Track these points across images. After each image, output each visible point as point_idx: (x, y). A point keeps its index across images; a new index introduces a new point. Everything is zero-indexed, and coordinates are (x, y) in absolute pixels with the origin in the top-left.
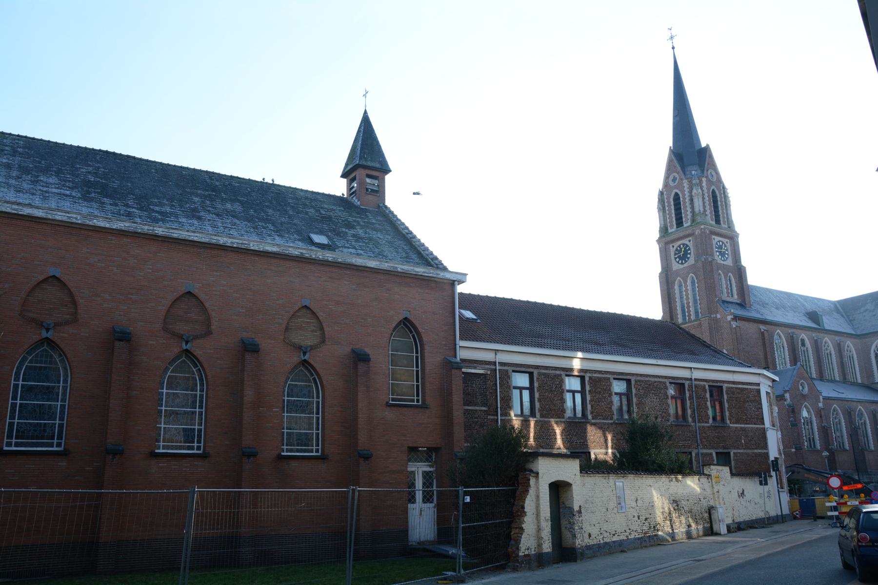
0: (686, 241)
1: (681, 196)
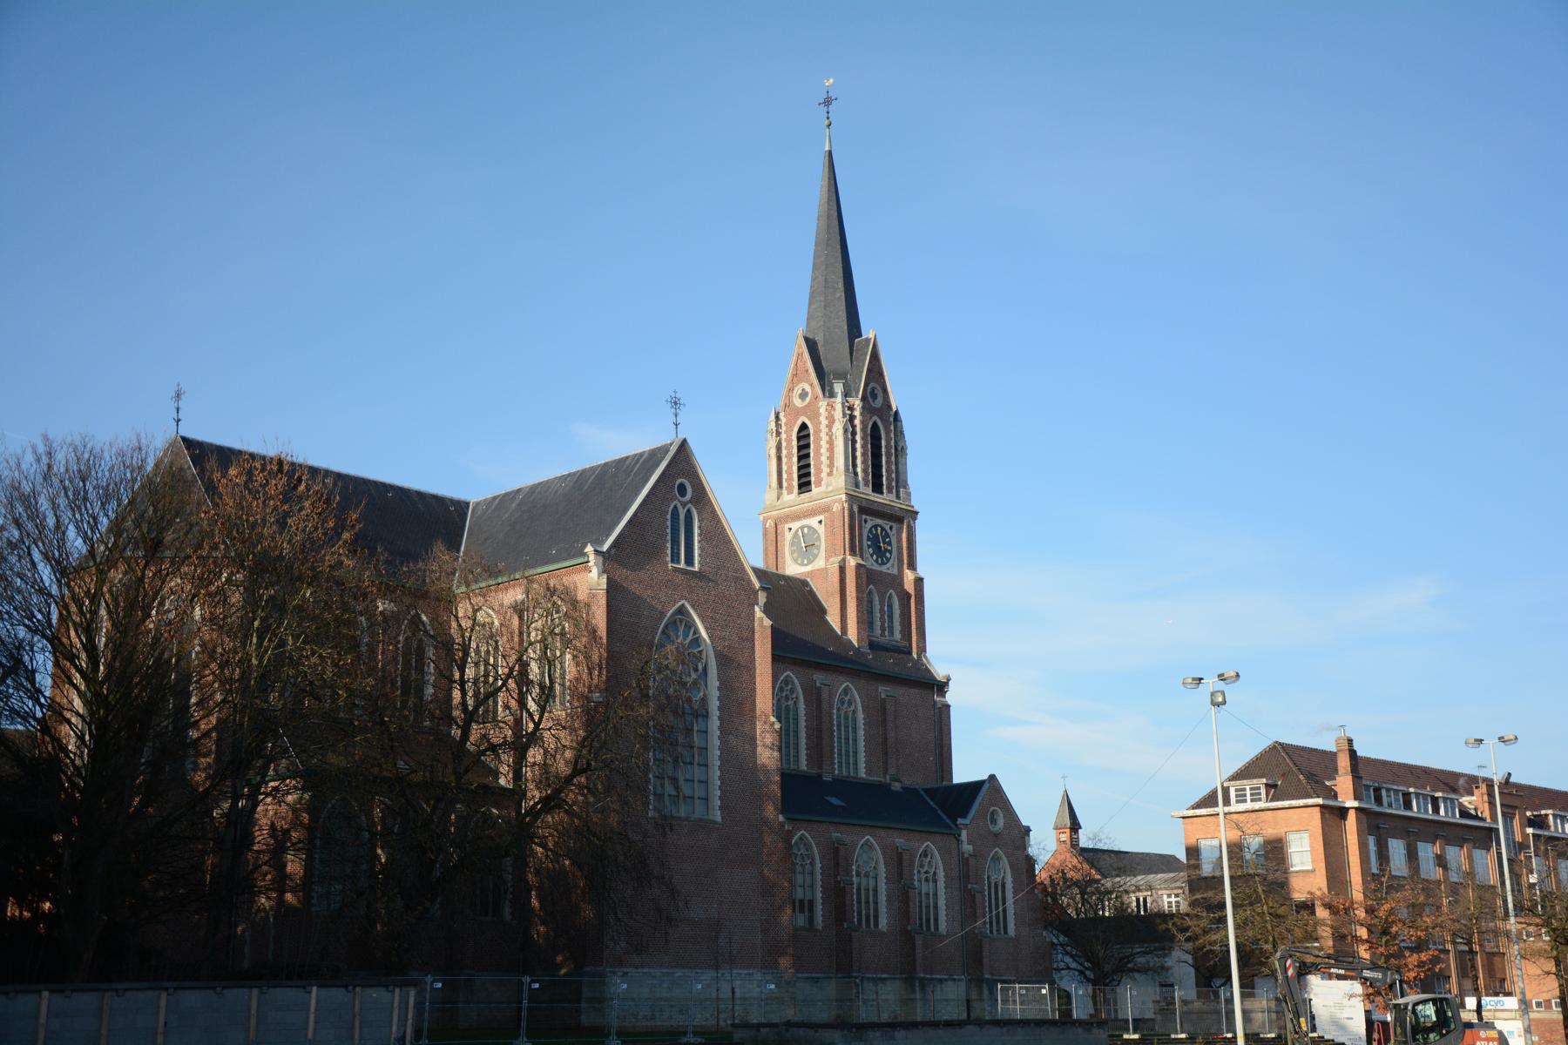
0: (813, 522)
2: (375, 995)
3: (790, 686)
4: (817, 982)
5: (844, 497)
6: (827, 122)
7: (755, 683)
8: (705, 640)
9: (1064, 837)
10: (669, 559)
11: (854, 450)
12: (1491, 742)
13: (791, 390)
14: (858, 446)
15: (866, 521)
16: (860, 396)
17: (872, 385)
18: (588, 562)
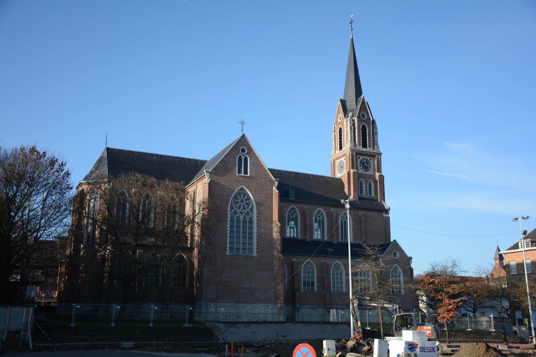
0: (342, 159)
2: (16, 310)
3: (294, 210)
4: (314, 309)
5: (349, 150)
6: (351, 29)
7: (273, 211)
8: (252, 198)
9: (498, 262)
10: (237, 172)
11: (354, 134)
12: (520, 219)
13: (337, 117)
14: (356, 133)
15: (359, 158)
16: (356, 117)
17: (362, 113)
18: (205, 175)
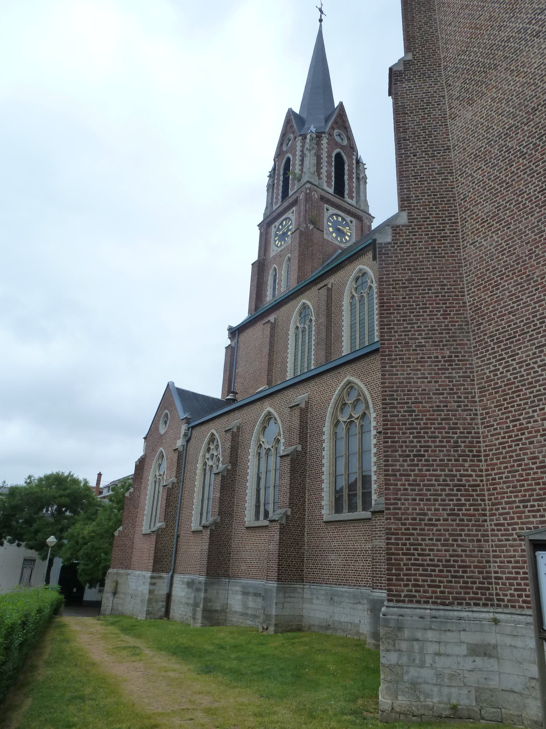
1: (291, 159)
